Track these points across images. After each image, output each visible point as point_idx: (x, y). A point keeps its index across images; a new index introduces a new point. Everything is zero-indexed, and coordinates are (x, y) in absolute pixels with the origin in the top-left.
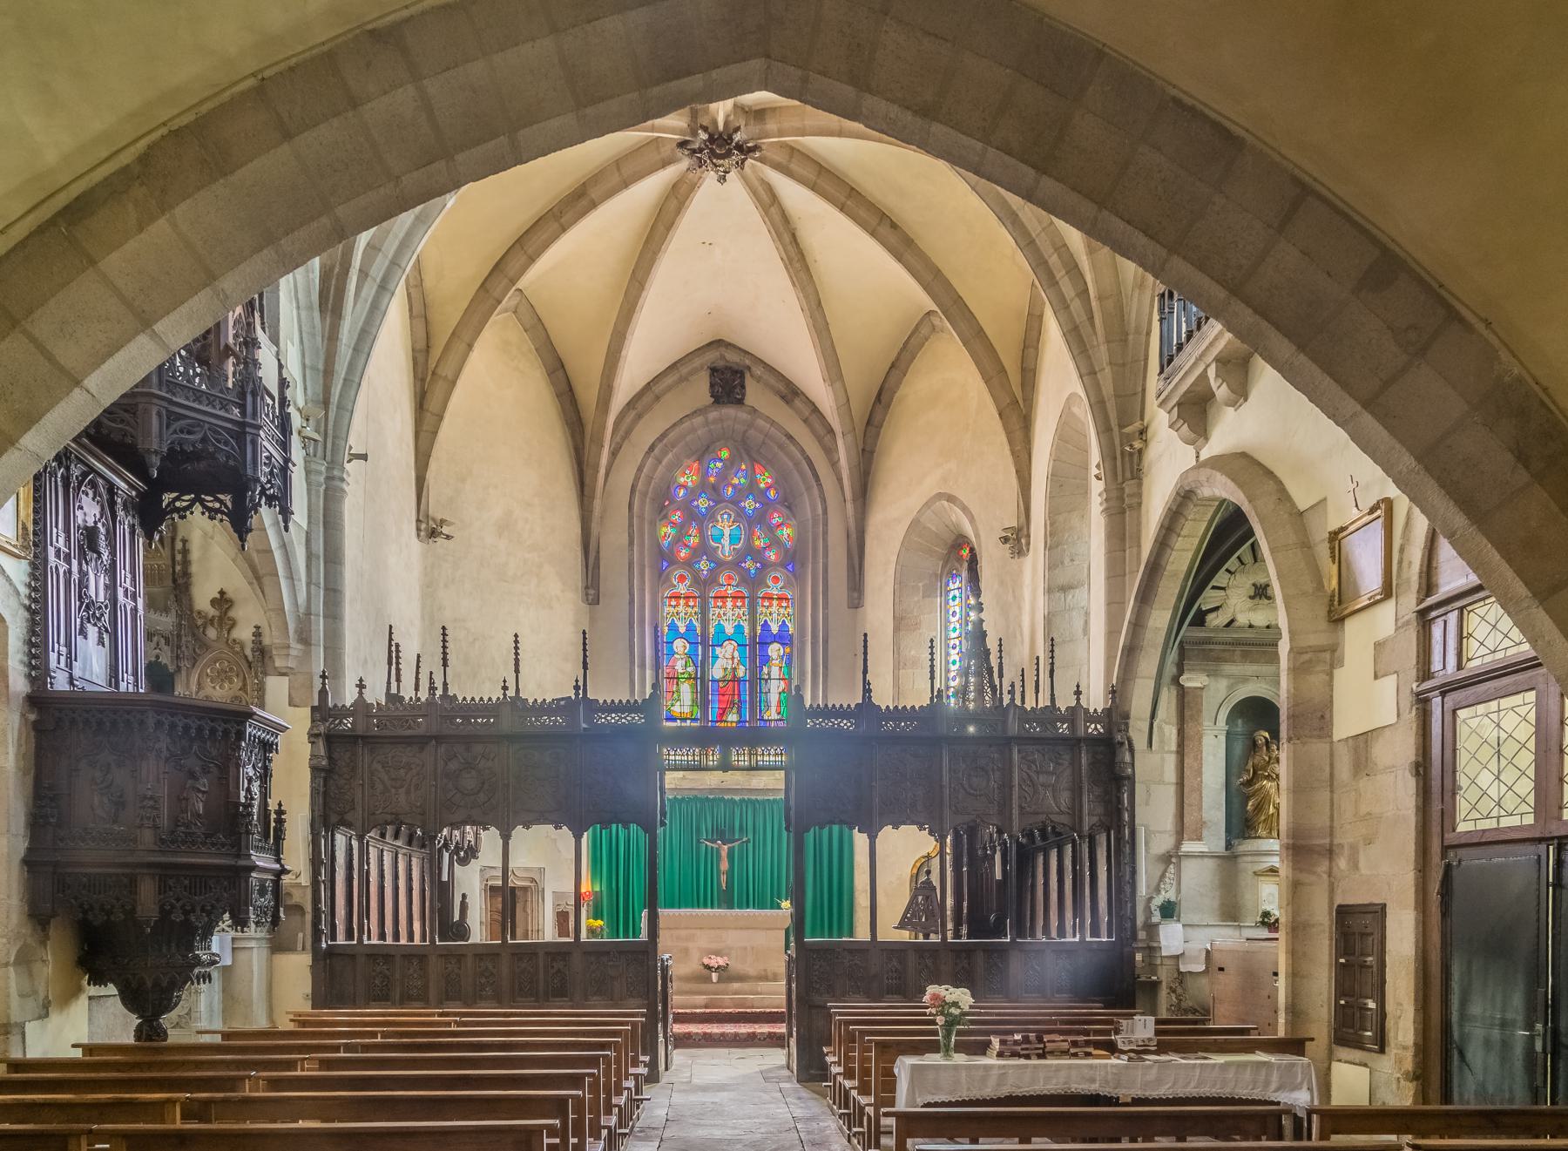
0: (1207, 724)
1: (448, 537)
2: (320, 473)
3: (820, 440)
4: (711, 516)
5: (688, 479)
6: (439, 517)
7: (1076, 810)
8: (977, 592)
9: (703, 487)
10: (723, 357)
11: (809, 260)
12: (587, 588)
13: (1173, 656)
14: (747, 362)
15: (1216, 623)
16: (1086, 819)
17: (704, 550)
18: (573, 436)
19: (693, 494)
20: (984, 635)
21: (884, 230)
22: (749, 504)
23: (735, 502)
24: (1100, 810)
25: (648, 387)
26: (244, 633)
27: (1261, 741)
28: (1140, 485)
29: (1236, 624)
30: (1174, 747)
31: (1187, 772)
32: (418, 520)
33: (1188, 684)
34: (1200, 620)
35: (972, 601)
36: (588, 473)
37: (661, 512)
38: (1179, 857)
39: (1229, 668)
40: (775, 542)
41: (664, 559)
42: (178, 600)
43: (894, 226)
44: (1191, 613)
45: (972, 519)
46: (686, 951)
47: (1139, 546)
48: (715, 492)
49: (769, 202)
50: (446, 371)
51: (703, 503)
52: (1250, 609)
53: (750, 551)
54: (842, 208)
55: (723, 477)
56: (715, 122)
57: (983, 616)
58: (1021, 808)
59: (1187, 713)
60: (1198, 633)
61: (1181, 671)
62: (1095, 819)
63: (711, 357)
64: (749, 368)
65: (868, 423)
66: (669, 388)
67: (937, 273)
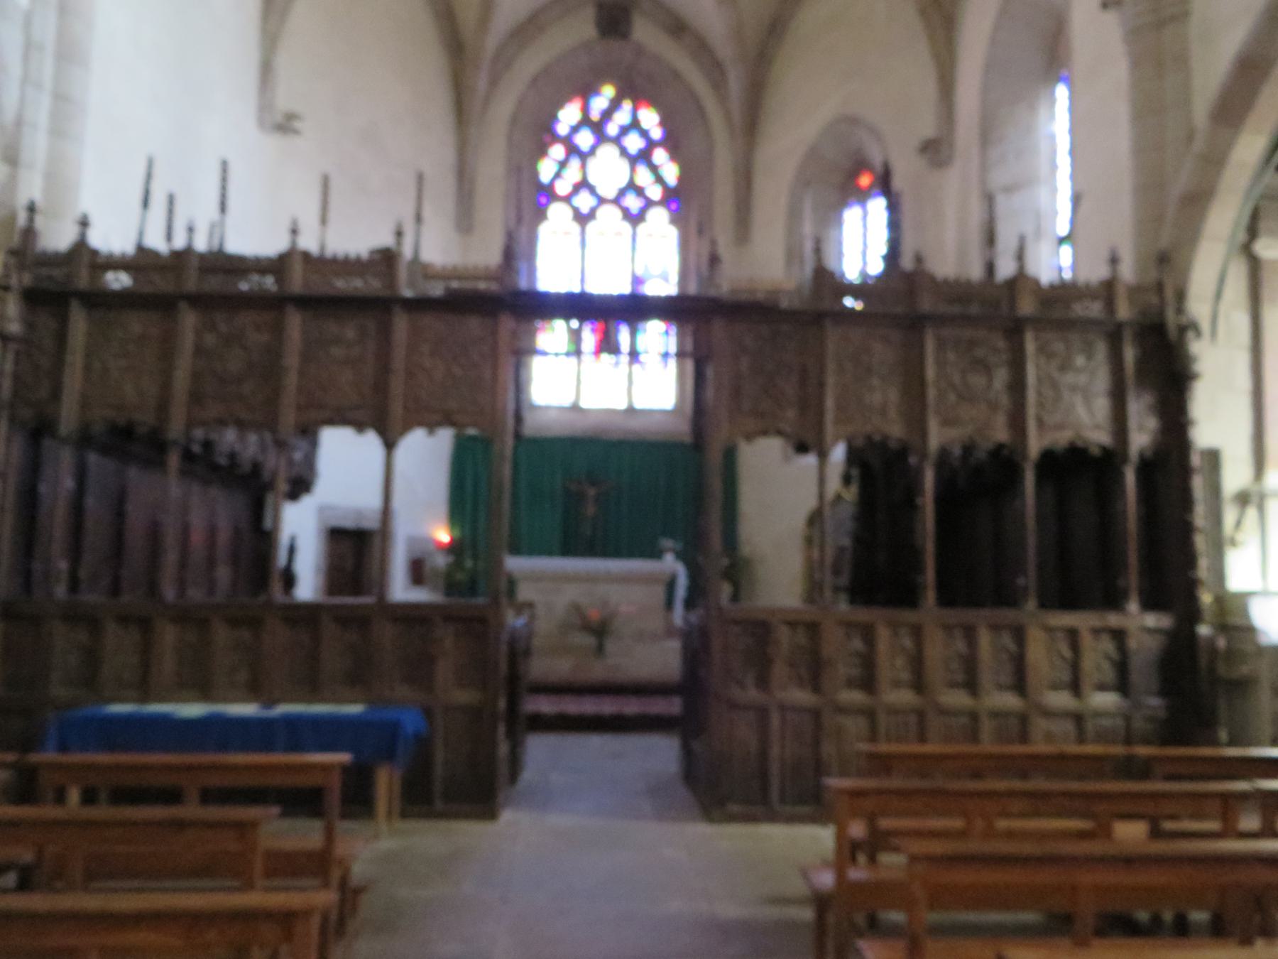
9: (586, 121)
17: (584, 184)
23: (617, 140)
51: (585, 139)
53: (632, 187)
55: (607, 115)
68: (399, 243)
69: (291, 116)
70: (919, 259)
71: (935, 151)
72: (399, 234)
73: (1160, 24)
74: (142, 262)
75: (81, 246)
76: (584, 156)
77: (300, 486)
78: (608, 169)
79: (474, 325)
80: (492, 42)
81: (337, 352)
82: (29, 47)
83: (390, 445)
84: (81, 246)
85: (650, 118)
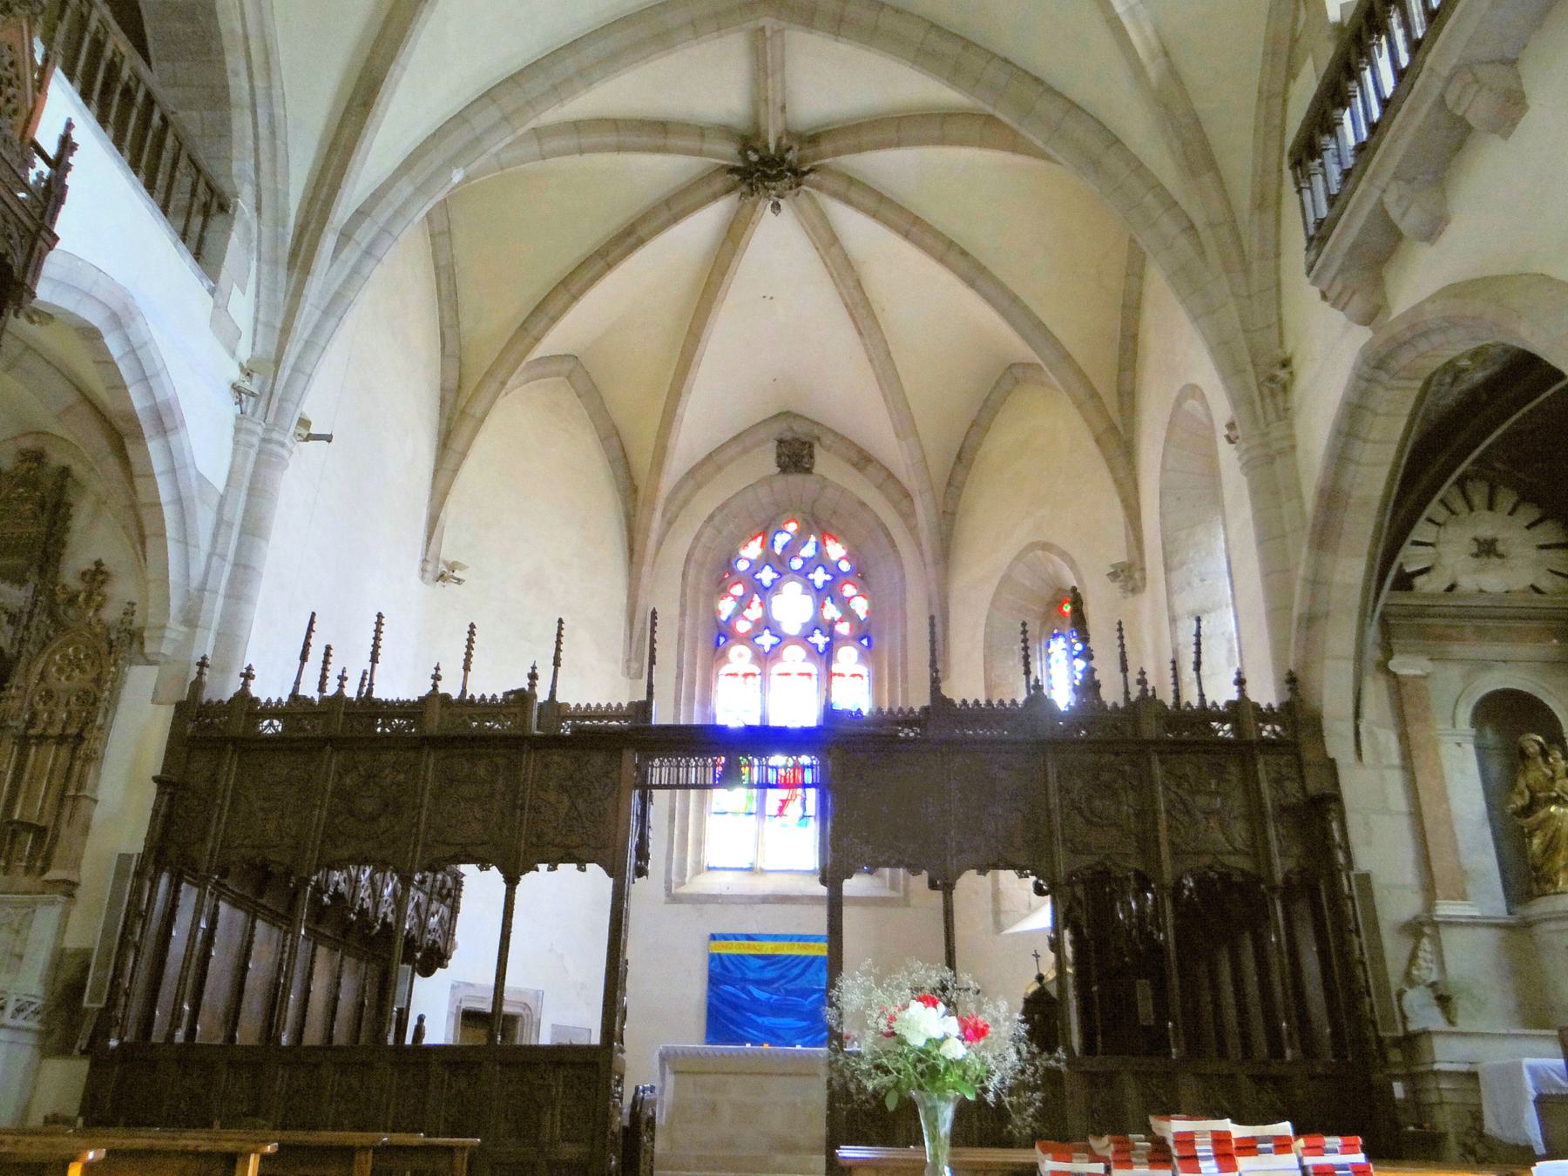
0: (1442, 726)
1: (459, 581)
2: (253, 433)
3: (895, 505)
4: (775, 587)
5: (753, 550)
6: (451, 560)
7: (1258, 847)
8: (1084, 639)
9: (768, 559)
10: (791, 429)
11: (875, 307)
12: (629, 661)
13: (1373, 632)
14: (816, 431)
15: (1428, 588)
16: (1277, 861)
17: (766, 623)
18: (625, 503)
19: (756, 566)
20: (1096, 686)
21: (952, 257)
22: (819, 577)
23: (804, 573)
24: (1296, 850)
25: (710, 457)
26: (111, 614)
27: (1533, 749)
28: (1290, 426)
29: (1456, 592)
30: (1396, 760)
31: (1424, 796)
32: (425, 561)
33: (1403, 672)
34: (1405, 582)
35: (1079, 647)
36: (638, 538)
37: (722, 590)
38: (1435, 925)
39: (1457, 649)
40: (849, 614)
41: (722, 635)
42: (42, 571)
43: (964, 253)
44: (1390, 574)
45: (1072, 564)
46: (713, 1108)
47: (1300, 497)
48: (780, 565)
49: (828, 241)
50: (477, 410)
51: (767, 576)
52: (1476, 571)
53: (816, 624)
54: (906, 235)
55: (791, 549)
56: (767, 147)
57: (1093, 664)
58: (1172, 844)
59: (1408, 709)
60: (1403, 598)
61: (1388, 652)
62: (1291, 864)
63: (778, 429)
64: (819, 439)
65: (949, 484)
66: (732, 460)
67: (1015, 299)
68: (532, 686)
69: (453, 567)
70: (129, 611)
71: (1128, 576)
72: (533, 677)
73: (1270, 460)
74: (296, 708)
75: (243, 695)
76: (765, 592)
77: (433, 958)
78: (793, 606)
79: (598, 760)
80: (667, 484)
81: (467, 790)
82: (220, 522)
83: (512, 882)
84: (243, 695)
85: (835, 550)
